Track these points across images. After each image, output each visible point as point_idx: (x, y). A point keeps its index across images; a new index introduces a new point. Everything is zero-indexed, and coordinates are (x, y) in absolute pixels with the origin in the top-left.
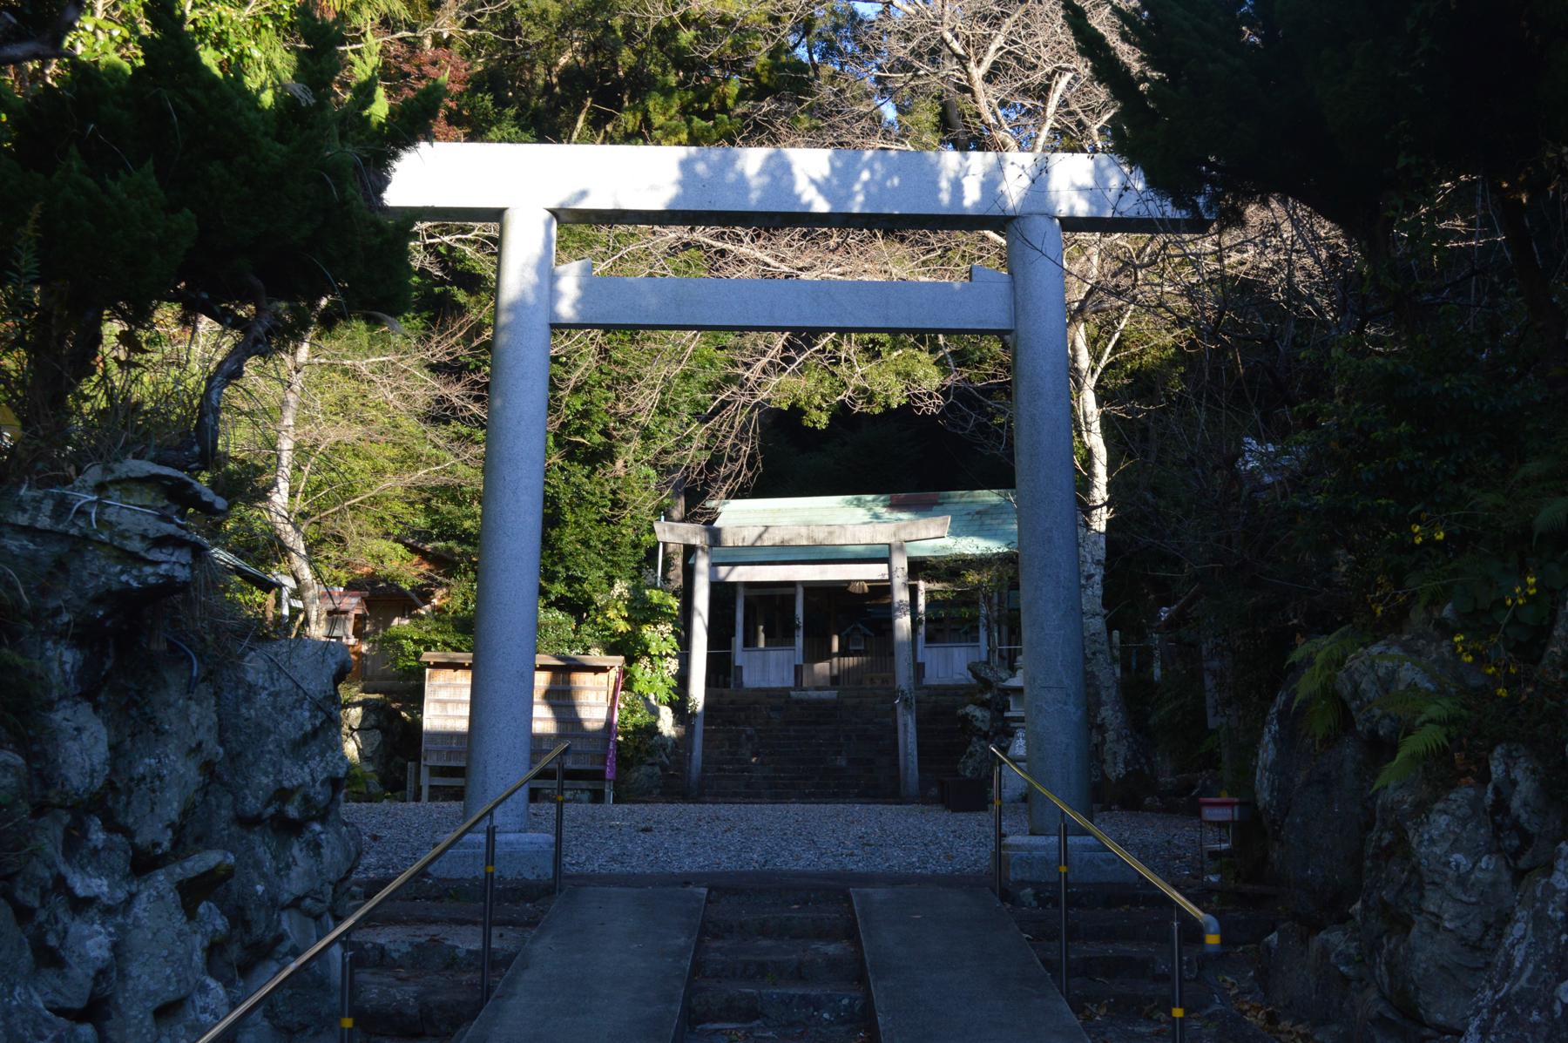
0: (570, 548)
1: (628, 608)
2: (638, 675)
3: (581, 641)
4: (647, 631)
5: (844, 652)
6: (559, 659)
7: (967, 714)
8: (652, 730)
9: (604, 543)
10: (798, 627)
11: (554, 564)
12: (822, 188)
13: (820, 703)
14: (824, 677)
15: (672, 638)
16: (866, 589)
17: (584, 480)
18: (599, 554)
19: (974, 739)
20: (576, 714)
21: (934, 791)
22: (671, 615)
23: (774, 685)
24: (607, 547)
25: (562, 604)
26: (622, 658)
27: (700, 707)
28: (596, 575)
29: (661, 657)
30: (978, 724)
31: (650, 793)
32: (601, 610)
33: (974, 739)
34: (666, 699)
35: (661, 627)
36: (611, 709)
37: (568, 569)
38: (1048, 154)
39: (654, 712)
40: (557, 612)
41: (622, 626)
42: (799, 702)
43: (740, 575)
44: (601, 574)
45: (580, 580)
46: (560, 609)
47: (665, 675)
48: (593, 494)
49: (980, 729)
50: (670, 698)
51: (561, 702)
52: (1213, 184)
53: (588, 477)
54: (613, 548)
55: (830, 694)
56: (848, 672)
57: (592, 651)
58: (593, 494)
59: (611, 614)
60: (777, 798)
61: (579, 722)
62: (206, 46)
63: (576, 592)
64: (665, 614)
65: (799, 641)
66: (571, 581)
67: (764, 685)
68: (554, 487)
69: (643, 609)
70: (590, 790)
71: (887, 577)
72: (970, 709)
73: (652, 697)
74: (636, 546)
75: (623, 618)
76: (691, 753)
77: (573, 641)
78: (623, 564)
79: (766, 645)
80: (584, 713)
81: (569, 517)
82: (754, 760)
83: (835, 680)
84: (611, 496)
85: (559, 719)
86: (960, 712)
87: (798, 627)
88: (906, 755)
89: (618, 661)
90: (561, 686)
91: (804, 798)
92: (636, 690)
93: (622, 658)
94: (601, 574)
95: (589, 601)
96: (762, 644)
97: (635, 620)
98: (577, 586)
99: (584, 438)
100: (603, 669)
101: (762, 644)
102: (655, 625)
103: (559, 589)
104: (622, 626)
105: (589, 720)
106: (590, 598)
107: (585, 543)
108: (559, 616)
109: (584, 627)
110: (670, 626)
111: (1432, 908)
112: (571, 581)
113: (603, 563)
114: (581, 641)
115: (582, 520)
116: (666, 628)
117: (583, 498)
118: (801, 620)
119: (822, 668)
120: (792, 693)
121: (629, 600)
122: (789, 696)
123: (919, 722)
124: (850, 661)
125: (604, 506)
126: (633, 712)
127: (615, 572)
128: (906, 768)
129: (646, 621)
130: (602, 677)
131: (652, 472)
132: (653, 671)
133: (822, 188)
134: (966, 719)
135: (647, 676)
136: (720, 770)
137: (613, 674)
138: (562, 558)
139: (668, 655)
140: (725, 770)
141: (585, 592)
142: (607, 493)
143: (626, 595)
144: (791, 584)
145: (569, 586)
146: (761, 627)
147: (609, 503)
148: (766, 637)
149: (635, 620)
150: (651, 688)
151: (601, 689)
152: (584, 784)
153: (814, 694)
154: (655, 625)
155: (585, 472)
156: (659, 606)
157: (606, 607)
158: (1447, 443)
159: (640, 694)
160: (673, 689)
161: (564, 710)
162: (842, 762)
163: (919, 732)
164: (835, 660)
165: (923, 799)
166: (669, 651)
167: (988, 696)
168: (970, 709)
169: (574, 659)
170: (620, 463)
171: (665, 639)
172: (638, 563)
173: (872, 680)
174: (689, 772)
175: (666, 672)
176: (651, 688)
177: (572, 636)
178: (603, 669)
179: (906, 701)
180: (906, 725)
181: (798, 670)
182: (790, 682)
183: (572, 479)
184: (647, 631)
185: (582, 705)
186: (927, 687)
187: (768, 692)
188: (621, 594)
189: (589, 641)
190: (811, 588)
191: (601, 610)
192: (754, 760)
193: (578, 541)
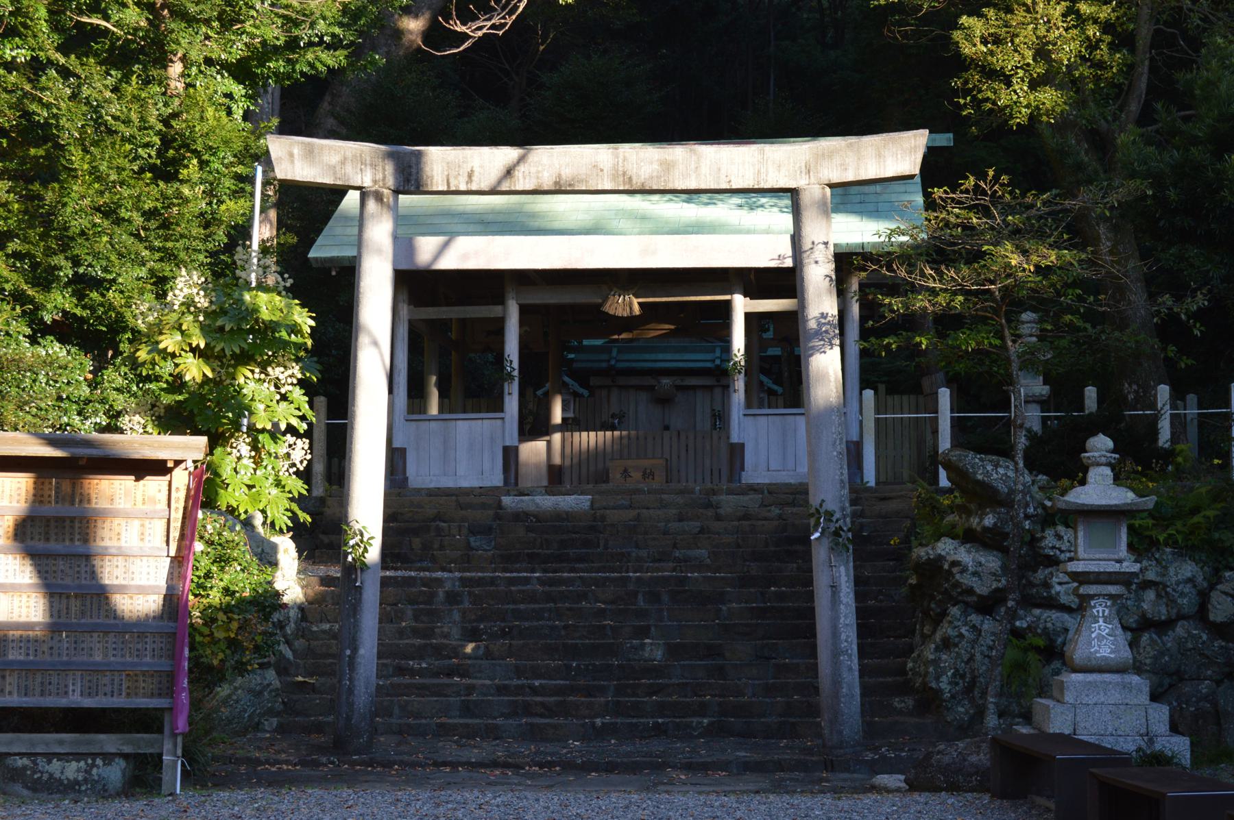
0: (77, 224)
1: (205, 330)
2: (226, 472)
3: (103, 401)
4: (249, 382)
5: (568, 425)
6: (52, 442)
7: (940, 558)
8: (268, 601)
9: (149, 215)
10: (510, 377)
11: (49, 252)
14: (537, 466)
15: (298, 394)
16: (637, 310)
17: (108, 94)
18: (137, 236)
19: (955, 611)
20: (93, 574)
22: (299, 346)
23: (465, 484)
24: (153, 224)
25: (66, 331)
26: (203, 440)
27: (373, 554)
28: (130, 275)
29: (275, 434)
30: (967, 580)
31: (257, 727)
32: (150, 337)
33: (955, 611)
34: (283, 520)
35: (276, 372)
36: (179, 561)
37: (76, 262)
39: (267, 557)
40: (57, 346)
41: (194, 370)
42: (520, 517)
43: (465, 257)
44: (143, 272)
45: (99, 284)
46: (63, 340)
47: (283, 475)
48: (128, 122)
49: (970, 591)
50: (294, 518)
51: (54, 546)
53: (115, 90)
54: (166, 225)
55: (574, 502)
56: (594, 456)
57: (124, 422)
58: (128, 122)
59: (170, 342)
61: (100, 595)
63: (93, 309)
64: (285, 344)
66: (82, 284)
67: (448, 483)
68: (48, 106)
69: (239, 332)
70: (125, 756)
71: (789, 263)
72: (946, 547)
73: (258, 520)
74: (208, 221)
75: (194, 350)
76: (355, 650)
77: (88, 402)
78: (182, 255)
79: (441, 410)
80: (111, 573)
81: (76, 158)
82: (469, 648)
83: (556, 476)
84: (160, 126)
85: (52, 589)
86: (921, 553)
87: (510, 377)
88: (836, 653)
89: (191, 447)
90: (51, 509)
92: (223, 504)
93: (203, 440)
94: (143, 272)
95: (118, 325)
96: (434, 409)
97: (221, 357)
98: (94, 295)
99: (107, 18)
100: (159, 468)
101: (434, 409)
102: (264, 367)
103: (58, 302)
104: (194, 370)
105: (122, 589)
106: (120, 317)
107: (109, 212)
108: (55, 349)
109: (109, 373)
110: (296, 370)
111: (1071, 701)
112: (82, 284)
113: (146, 253)
114: (103, 401)
115: (103, 167)
116: (288, 373)
117: (111, 132)
118: (516, 365)
119: (534, 451)
120: (507, 500)
121: (207, 314)
122: (499, 506)
124: (588, 439)
125: (147, 145)
126: (222, 561)
127: (166, 269)
128: (837, 683)
129: (244, 358)
130: (154, 485)
131: (238, 90)
132: (257, 462)
135: (246, 475)
136: (401, 671)
137: (181, 478)
138: (65, 243)
139: (291, 430)
140: (413, 672)
141: (111, 307)
142: (152, 120)
143: (202, 302)
145: (80, 296)
146: (434, 379)
147: (156, 140)
148: (442, 396)
149: (221, 357)
150: (255, 499)
151: (149, 516)
152: (109, 742)
154: (264, 367)
155: (110, 81)
156: (272, 326)
157: (158, 329)
158: (225, 383)
159: (231, 511)
160: (300, 500)
161: (61, 565)
162: (653, 651)
164: (557, 437)
166: (295, 422)
167: (989, 521)
168: (946, 547)
169: (88, 443)
170: (176, 69)
171: (284, 398)
172: (212, 254)
173: (625, 472)
174: (350, 691)
175: (283, 465)
176: (255, 499)
177: (85, 391)
178: (159, 468)
180: (834, 588)
182: (497, 479)
183: (86, 92)
184: (249, 382)
185: (113, 514)
186: (754, 489)
188: (189, 304)
189: (120, 401)
191: (150, 337)
192: (469, 648)
193: (98, 209)
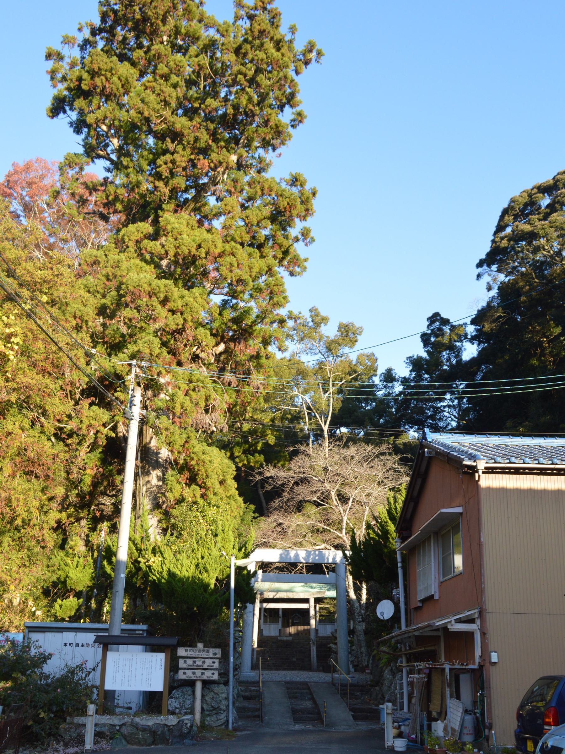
12: (304, 559)
13: (287, 641)
21: (321, 668)
38: (186, 6)
42: (281, 641)
52: (459, 405)
60: (277, 669)
62: (207, 106)
65: (281, 620)
91: (284, 669)
123: (317, 648)
133: (304, 559)
134: (330, 648)
144: (278, 609)
153: (285, 638)
162: (295, 659)
163: (317, 651)
165: (318, 670)
179: (313, 643)
181: (280, 630)
182: (278, 634)
187: (271, 637)
190: (284, 610)
